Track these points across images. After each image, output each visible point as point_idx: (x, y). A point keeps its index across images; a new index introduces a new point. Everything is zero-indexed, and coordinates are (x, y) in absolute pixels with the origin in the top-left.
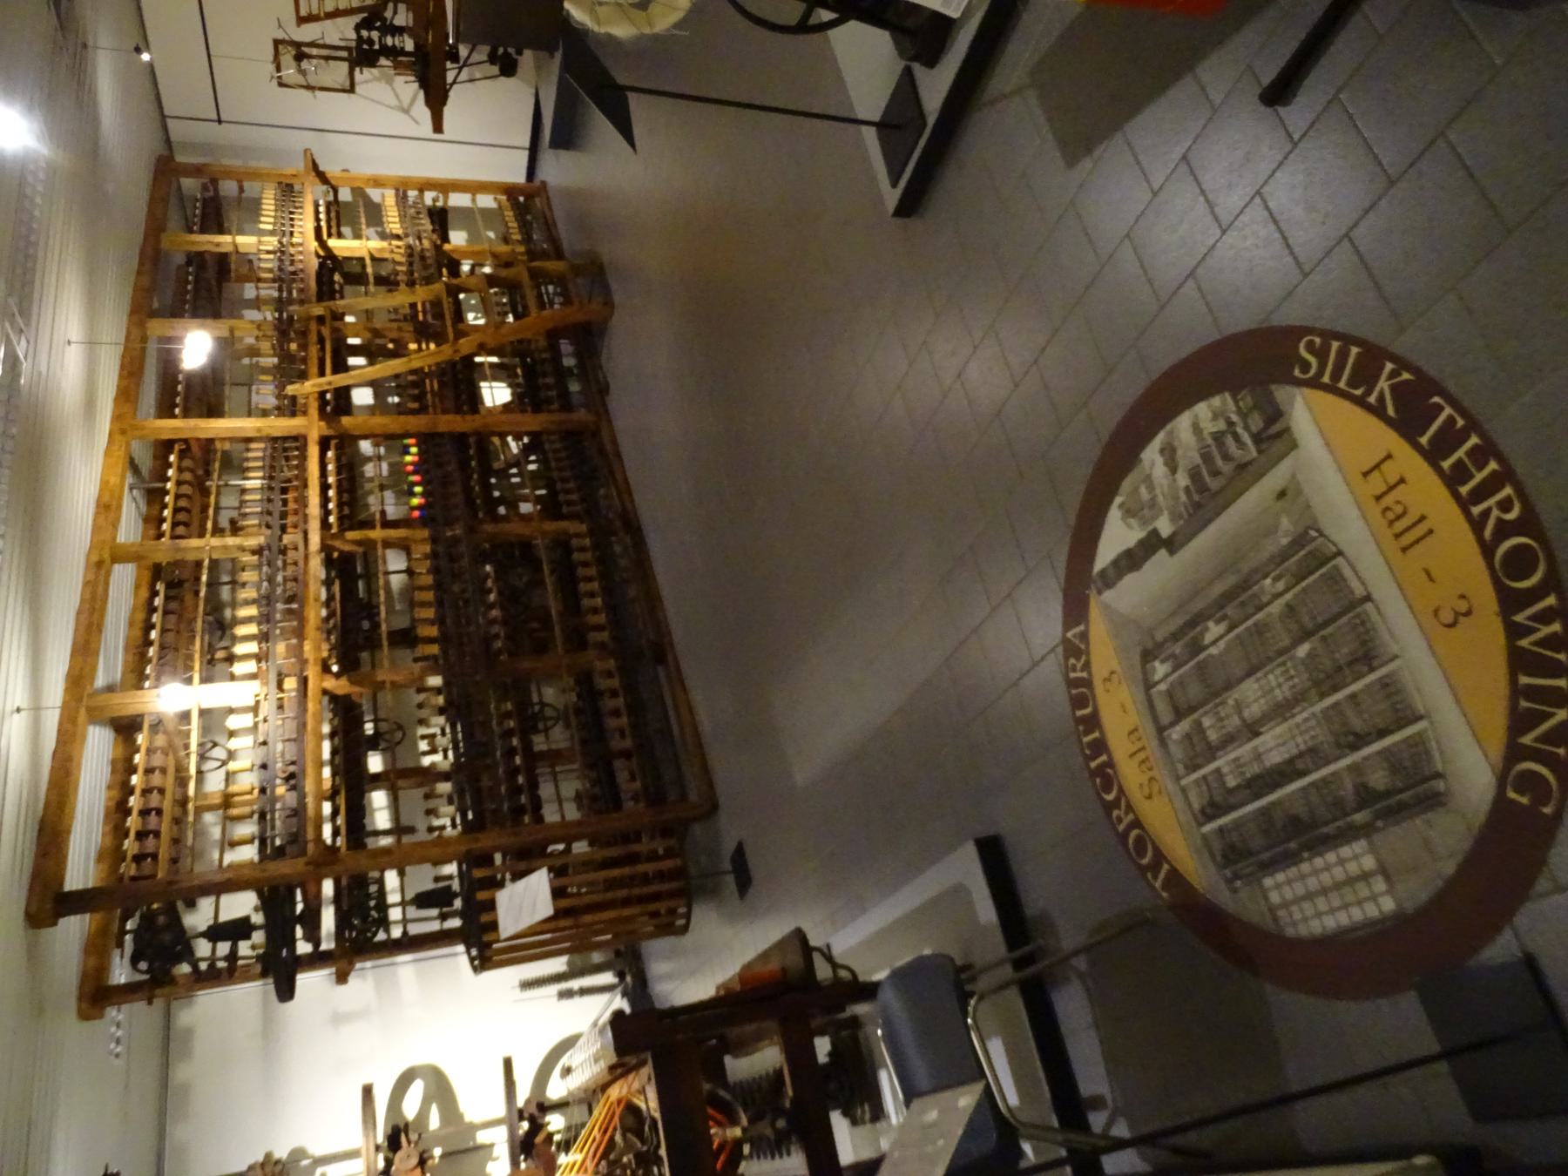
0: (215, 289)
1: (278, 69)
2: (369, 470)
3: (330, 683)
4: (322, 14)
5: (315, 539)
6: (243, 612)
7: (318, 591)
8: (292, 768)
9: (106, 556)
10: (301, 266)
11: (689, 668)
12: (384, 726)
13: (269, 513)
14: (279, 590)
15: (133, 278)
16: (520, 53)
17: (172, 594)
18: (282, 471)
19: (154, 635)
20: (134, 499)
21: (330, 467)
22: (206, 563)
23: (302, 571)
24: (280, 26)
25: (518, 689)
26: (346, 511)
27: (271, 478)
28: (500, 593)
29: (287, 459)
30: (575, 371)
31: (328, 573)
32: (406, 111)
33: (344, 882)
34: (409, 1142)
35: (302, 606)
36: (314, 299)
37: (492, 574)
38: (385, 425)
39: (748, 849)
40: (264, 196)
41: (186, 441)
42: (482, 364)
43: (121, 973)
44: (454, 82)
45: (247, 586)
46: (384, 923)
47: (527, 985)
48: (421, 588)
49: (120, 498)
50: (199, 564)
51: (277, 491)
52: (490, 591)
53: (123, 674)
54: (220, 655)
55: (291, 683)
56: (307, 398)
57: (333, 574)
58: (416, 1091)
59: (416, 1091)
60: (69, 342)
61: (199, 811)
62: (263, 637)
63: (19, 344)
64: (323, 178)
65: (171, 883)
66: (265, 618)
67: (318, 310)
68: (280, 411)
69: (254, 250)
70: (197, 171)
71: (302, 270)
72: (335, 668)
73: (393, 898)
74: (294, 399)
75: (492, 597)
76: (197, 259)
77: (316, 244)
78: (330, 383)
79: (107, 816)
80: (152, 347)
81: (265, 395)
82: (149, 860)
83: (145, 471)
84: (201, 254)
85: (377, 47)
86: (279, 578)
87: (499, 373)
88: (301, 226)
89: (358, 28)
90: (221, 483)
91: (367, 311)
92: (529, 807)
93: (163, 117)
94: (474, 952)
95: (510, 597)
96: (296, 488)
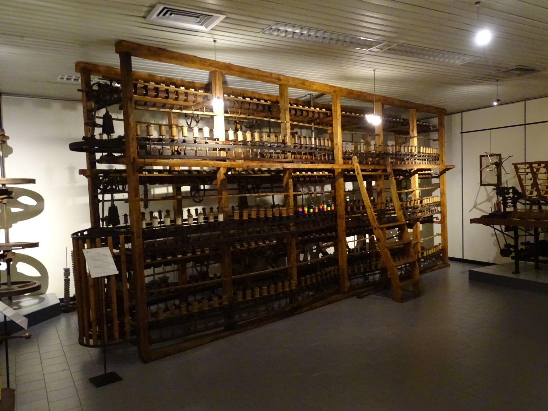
0: (394, 129)
1: (490, 155)
2: (318, 189)
3: (222, 171)
4: (519, 174)
5: (289, 166)
6: (257, 136)
7: (266, 166)
8: (183, 153)
9: (282, 82)
10: (406, 163)
11: (222, 344)
12: (202, 193)
13: (301, 147)
14: (266, 151)
15: (398, 98)
16: (513, 258)
17: (265, 107)
18: (319, 153)
19: (248, 99)
20: (306, 96)
21: (321, 173)
22: (279, 121)
23: (274, 160)
24: (510, 157)
25: (217, 257)
26: (301, 179)
27: (316, 149)
28: (263, 247)
29: (324, 155)
30: (367, 281)
31: (273, 171)
32: (475, 207)
33: (124, 175)
34: (2, 199)
35: (258, 160)
36: (394, 168)
37: (272, 243)
38: (340, 196)
39: (116, 384)
40: (434, 149)
41: (331, 115)
42: (365, 237)
43: (95, 79)
44: (495, 229)
45: (268, 138)
46: (104, 192)
47: (14, 289)
48: (266, 211)
49: (307, 89)
50: (279, 119)
51: (310, 151)
52: (264, 243)
53: (231, 88)
54: (239, 126)
55: (223, 154)
56: (351, 164)
57: (273, 173)
58: (31, 202)
59: (31, 202)
60: (374, 70)
61: (169, 114)
62: (245, 143)
63: (377, 48)
64: (443, 172)
65: (131, 100)
66: (253, 144)
67: (389, 170)
68: (345, 153)
69: (411, 145)
70: (441, 124)
71: (405, 163)
72: (230, 173)
73: (117, 196)
74: (351, 159)
75: (261, 243)
76: (406, 123)
77: (416, 169)
78: (358, 174)
79: (170, 79)
80: (369, 105)
81: (350, 148)
82: (145, 92)
83: (317, 100)
84: (408, 124)
85: (506, 196)
86: (272, 151)
87: (361, 243)
88: (423, 163)
89: (513, 188)
90: (313, 129)
91: (389, 189)
92: (155, 262)
93: (462, 112)
94: (86, 233)
95: (261, 252)
96: (312, 159)
